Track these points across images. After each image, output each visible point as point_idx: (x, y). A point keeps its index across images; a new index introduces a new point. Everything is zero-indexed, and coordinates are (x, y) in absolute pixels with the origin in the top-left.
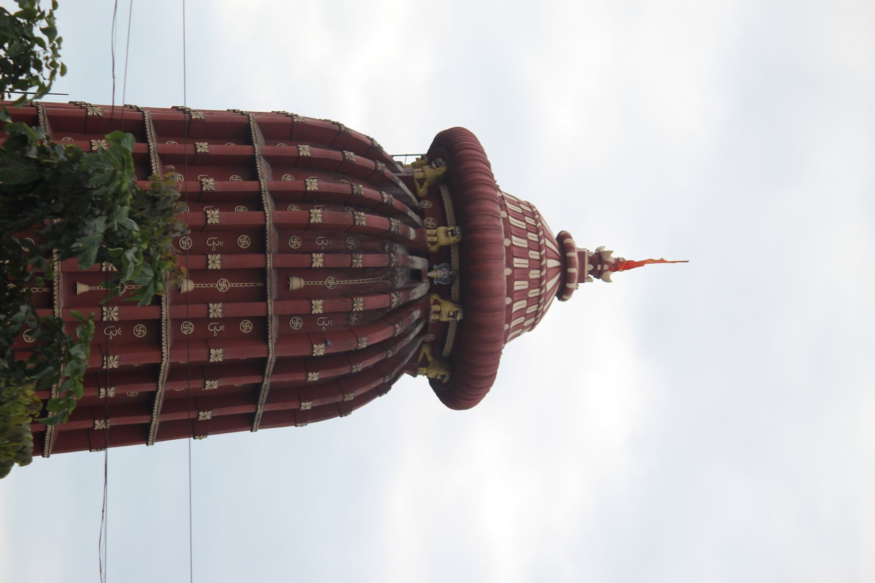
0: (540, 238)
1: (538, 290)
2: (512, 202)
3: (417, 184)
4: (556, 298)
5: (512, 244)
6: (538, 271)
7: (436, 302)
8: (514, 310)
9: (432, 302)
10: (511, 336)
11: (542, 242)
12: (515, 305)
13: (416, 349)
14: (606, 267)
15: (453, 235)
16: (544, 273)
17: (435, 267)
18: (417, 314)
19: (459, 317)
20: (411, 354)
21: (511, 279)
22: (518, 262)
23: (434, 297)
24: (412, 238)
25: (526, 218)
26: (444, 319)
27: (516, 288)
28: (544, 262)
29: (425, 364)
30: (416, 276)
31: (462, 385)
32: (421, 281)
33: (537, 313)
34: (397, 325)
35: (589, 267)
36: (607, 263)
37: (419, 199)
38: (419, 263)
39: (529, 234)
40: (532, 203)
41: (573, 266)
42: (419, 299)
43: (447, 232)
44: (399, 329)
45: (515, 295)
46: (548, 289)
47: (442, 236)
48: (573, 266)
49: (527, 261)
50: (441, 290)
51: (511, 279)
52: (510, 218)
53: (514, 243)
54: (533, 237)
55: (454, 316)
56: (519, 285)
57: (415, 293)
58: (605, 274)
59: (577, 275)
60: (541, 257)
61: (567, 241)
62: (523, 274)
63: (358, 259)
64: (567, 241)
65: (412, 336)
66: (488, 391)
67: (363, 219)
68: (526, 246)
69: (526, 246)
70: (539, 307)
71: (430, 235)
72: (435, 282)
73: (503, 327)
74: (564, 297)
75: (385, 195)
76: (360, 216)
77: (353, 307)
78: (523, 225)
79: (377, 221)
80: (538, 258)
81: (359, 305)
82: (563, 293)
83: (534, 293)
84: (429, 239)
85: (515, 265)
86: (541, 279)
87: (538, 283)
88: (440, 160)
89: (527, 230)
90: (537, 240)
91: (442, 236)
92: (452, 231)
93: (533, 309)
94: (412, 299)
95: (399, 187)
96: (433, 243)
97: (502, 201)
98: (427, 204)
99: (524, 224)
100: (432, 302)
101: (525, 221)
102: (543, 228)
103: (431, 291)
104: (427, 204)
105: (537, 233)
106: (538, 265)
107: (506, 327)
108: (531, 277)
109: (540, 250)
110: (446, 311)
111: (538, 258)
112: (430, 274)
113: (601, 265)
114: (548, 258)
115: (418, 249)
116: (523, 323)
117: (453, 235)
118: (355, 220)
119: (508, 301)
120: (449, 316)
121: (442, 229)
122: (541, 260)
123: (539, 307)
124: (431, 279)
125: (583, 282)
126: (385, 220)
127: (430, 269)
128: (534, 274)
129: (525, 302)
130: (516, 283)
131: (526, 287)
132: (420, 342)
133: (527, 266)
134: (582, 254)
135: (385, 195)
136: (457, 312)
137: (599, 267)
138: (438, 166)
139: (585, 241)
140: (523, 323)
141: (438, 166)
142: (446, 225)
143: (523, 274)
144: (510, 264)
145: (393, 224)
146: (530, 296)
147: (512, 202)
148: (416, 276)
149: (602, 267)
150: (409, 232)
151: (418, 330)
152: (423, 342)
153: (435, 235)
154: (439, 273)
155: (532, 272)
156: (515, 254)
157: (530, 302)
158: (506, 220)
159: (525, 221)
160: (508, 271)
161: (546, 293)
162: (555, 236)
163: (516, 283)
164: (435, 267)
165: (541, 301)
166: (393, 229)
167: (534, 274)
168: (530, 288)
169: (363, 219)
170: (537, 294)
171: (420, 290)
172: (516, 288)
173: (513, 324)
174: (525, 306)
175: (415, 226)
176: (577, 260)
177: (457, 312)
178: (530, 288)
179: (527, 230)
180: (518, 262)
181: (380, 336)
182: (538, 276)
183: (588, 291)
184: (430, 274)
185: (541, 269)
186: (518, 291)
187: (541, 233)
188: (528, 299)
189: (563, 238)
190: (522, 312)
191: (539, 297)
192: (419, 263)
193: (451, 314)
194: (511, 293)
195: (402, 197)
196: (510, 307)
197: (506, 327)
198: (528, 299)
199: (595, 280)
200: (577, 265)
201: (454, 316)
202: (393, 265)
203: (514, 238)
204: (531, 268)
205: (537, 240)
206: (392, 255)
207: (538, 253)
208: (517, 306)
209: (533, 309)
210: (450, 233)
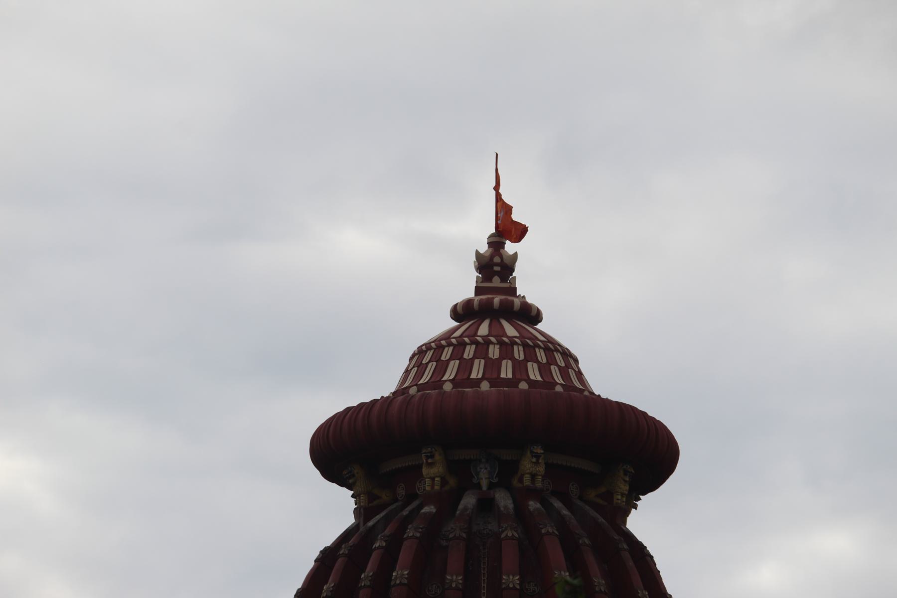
0: (450, 344)
1: (515, 347)
2: (419, 375)
3: (376, 503)
4: (539, 326)
5: (451, 381)
6: (491, 347)
7: (521, 480)
8: (539, 378)
9: (520, 485)
10: (577, 384)
11: (454, 341)
12: (532, 377)
13: (587, 508)
14: (497, 260)
15: (432, 457)
16: (493, 339)
17: (475, 481)
18: (533, 505)
19: (540, 451)
20: (593, 513)
21: (496, 382)
22: (477, 372)
23: (515, 482)
24: (434, 511)
25: (424, 362)
26: (541, 469)
27: (510, 376)
28: (479, 339)
29: (609, 496)
30: (486, 505)
31: (643, 452)
32: (493, 499)
33: (547, 350)
34: (543, 531)
35: (496, 282)
36: (492, 257)
37: (396, 500)
38: (469, 501)
39: (443, 358)
40: (410, 355)
41: (496, 301)
42: (515, 502)
43: (430, 465)
44: (549, 528)
45: (518, 376)
46: (516, 334)
47: (433, 473)
48: (496, 301)
49: (477, 361)
50: (506, 475)
51: (496, 382)
52: (421, 382)
53: (452, 377)
54: (447, 354)
55: (538, 457)
56: (506, 371)
57: (506, 507)
58: (506, 261)
59: (503, 297)
60: (472, 343)
61: (459, 309)
62: (493, 366)
63: (452, 581)
64: (459, 309)
65: (565, 512)
66: (644, 414)
67: (401, 574)
68: (457, 362)
69: (457, 362)
70: (539, 347)
71: (433, 487)
72: (495, 480)
73: (558, 393)
74: (534, 313)
75: (377, 545)
76: (396, 578)
77: (514, 588)
78: (432, 366)
79: (405, 556)
80: (474, 347)
81: (512, 580)
82: (531, 315)
83: (519, 353)
84: (437, 487)
85: (480, 376)
86: (501, 343)
87: (507, 348)
88: (345, 472)
89: (461, 358)
90: (451, 348)
91: (433, 473)
92: (427, 457)
93: (541, 356)
94: (512, 511)
95: (374, 526)
96: (444, 482)
97: (401, 392)
98: (401, 491)
99: (452, 363)
100: (520, 485)
101: (448, 361)
102: (437, 341)
103: (509, 488)
104: (401, 491)
105: (443, 347)
106: (482, 348)
107: (559, 389)
108: (497, 356)
109: (465, 344)
110: (532, 467)
111: (474, 347)
112: (485, 488)
113: (495, 267)
114: (475, 334)
115: (448, 502)
116: (559, 367)
117: (432, 457)
118: (401, 584)
119: (523, 386)
120: (537, 463)
121: (425, 471)
122: (477, 343)
123: (539, 347)
124: (491, 486)
125: (516, 288)
126: (406, 544)
127: (478, 486)
128: (494, 352)
129: (529, 364)
130: (503, 375)
131: (510, 362)
132: (579, 503)
133: (483, 361)
134: (478, 290)
135: (377, 545)
136: (532, 452)
137: (497, 268)
138: (353, 476)
139: (465, 285)
140: (559, 367)
141: (353, 476)
142: (420, 467)
143: (493, 366)
144: (477, 383)
145: (411, 534)
146: (522, 357)
147: (419, 375)
148: (486, 505)
149: (497, 265)
150: (425, 514)
151: (557, 504)
152: (581, 498)
153: (433, 479)
154: (484, 477)
155: (491, 355)
156: (465, 377)
157: (531, 356)
158: (421, 388)
159: (448, 361)
160: (485, 386)
161: (521, 337)
162: (455, 324)
163: (503, 375)
164: (475, 481)
165: (531, 343)
166: (418, 535)
167: (494, 352)
168: (512, 358)
169: (401, 574)
170: (521, 348)
171: (504, 501)
172: (510, 376)
173: (559, 379)
174: (535, 365)
175: (421, 507)
176: (484, 297)
177: (532, 452)
178: (512, 358)
179: (461, 358)
180: (477, 372)
181: (555, 552)
182: (497, 347)
183: (528, 285)
184: (485, 488)
185: (488, 343)
186: (514, 374)
187: (443, 342)
188: (526, 360)
189: (462, 312)
190: (544, 369)
191: (525, 346)
192: (469, 501)
193: (534, 460)
194: (512, 383)
195: (387, 520)
196: (532, 384)
197: (559, 389)
198: (526, 360)
199: (514, 274)
200: (490, 296)
201: (538, 457)
202: (464, 535)
203: (445, 378)
204: (486, 357)
205: (451, 348)
206: (451, 536)
207: (468, 347)
208: (534, 374)
209: (558, 357)
210: (430, 461)
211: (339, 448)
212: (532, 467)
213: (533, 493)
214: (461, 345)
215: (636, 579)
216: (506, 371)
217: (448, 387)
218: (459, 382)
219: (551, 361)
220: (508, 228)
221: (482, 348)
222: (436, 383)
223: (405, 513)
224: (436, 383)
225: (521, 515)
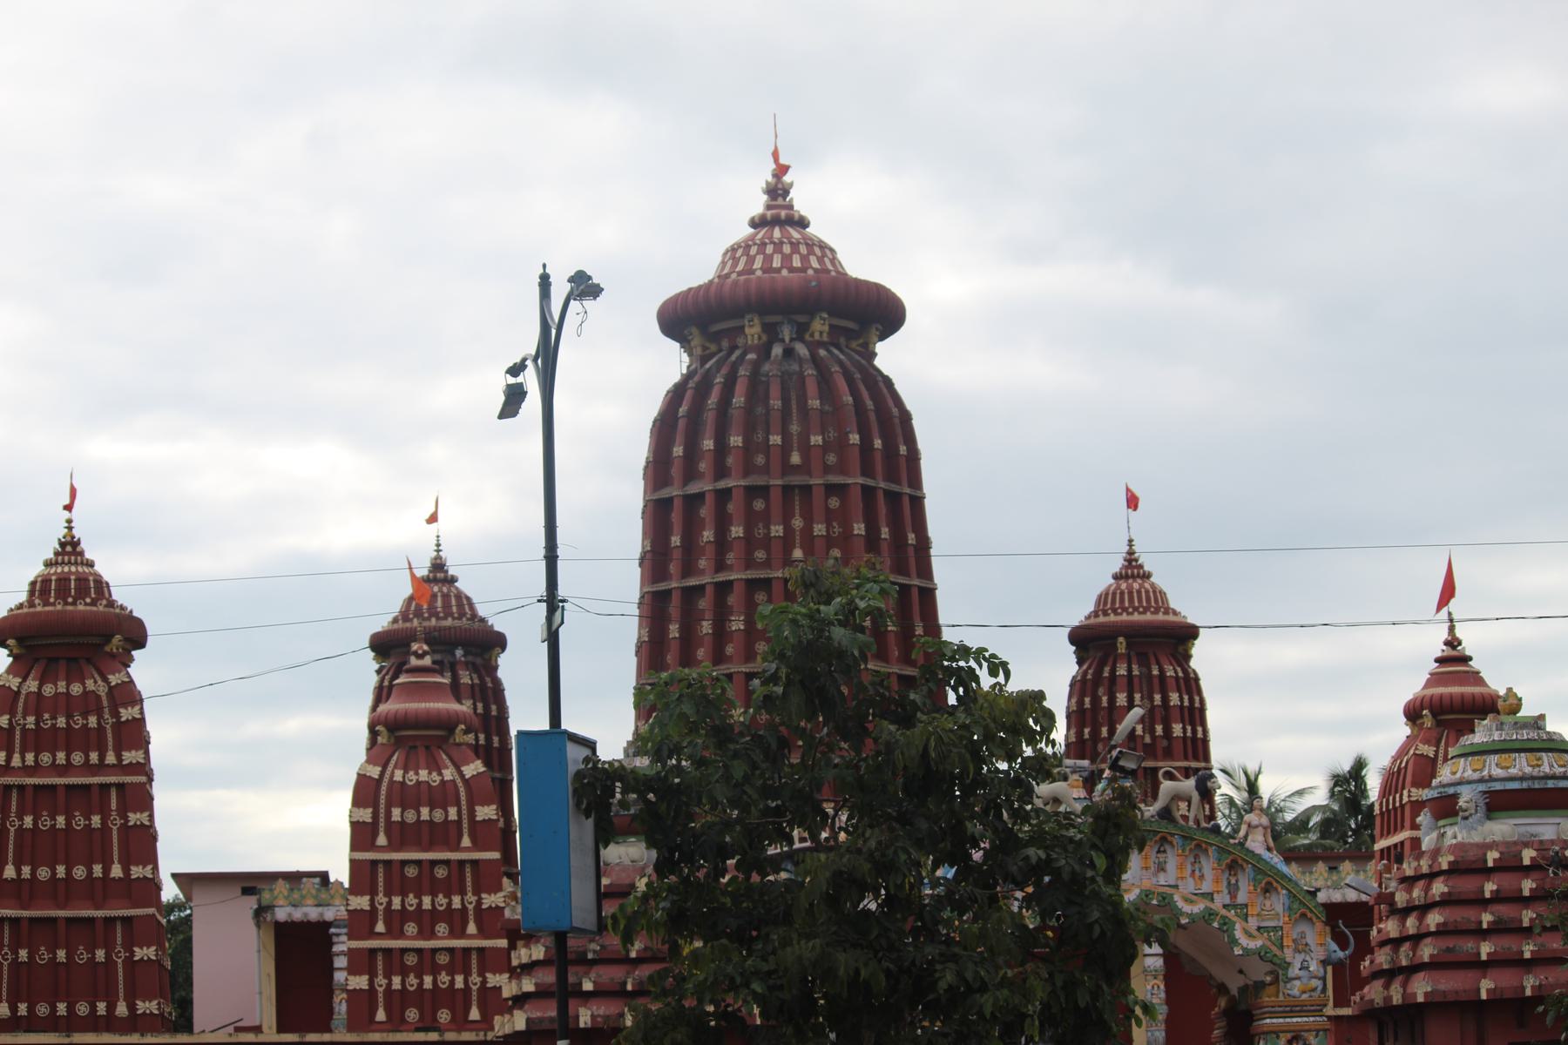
2: (735, 264)
7: (812, 335)
18: (822, 352)
21: (792, 270)
22: (777, 263)
23: (807, 337)
26: (826, 328)
30: (789, 353)
35: (780, 201)
38: (777, 350)
41: (779, 215)
44: (835, 368)
48: (779, 215)
50: (801, 331)
51: (792, 270)
56: (797, 262)
62: (787, 259)
67: (738, 400)
79: (740, 388)
81: (815, 403)
82: (802, 223)
86: (791, 243)
87: (795, 246)
91: (753, 331)
97: (722, 277)
98: (725, 344)
106: (778, 246)
113: (777, 191)
115: (765, 351)
119: (810, 272)
121: (747, 330)
124: (792, 340)
127: (783, 340)
128: (787, 249)
134: (769, 207)
139: (757, 204)
142: (743, 327)
144: (778, 270)
148: (789, 353)
151: (836, 352)
154: (786, 333)
158: (740, 274)
160: (785, 272)
167: (787, 249)
168: (781, 252)
169: (738, 400)
171: (802, 350)
180: (777, 263)
185: (782, 243)
189: (757, 223)
192: (777, 350)
194: (803, 270)
196: (816, 270)
204: (781, 252)
208: (815, 264)
211: (679, 319)
212: (820, 327)
213: (820, 344)
214: (764, 244)
215: (891, 403)
216: (797, 262)
217: (759, 273)
218: (767, 269)
219: (824, 255)
220: (781, 170)
221: (778, 246)
222: (749, 271)
223: (733, 358)
224: (749, 271)
225: (815, 359)
